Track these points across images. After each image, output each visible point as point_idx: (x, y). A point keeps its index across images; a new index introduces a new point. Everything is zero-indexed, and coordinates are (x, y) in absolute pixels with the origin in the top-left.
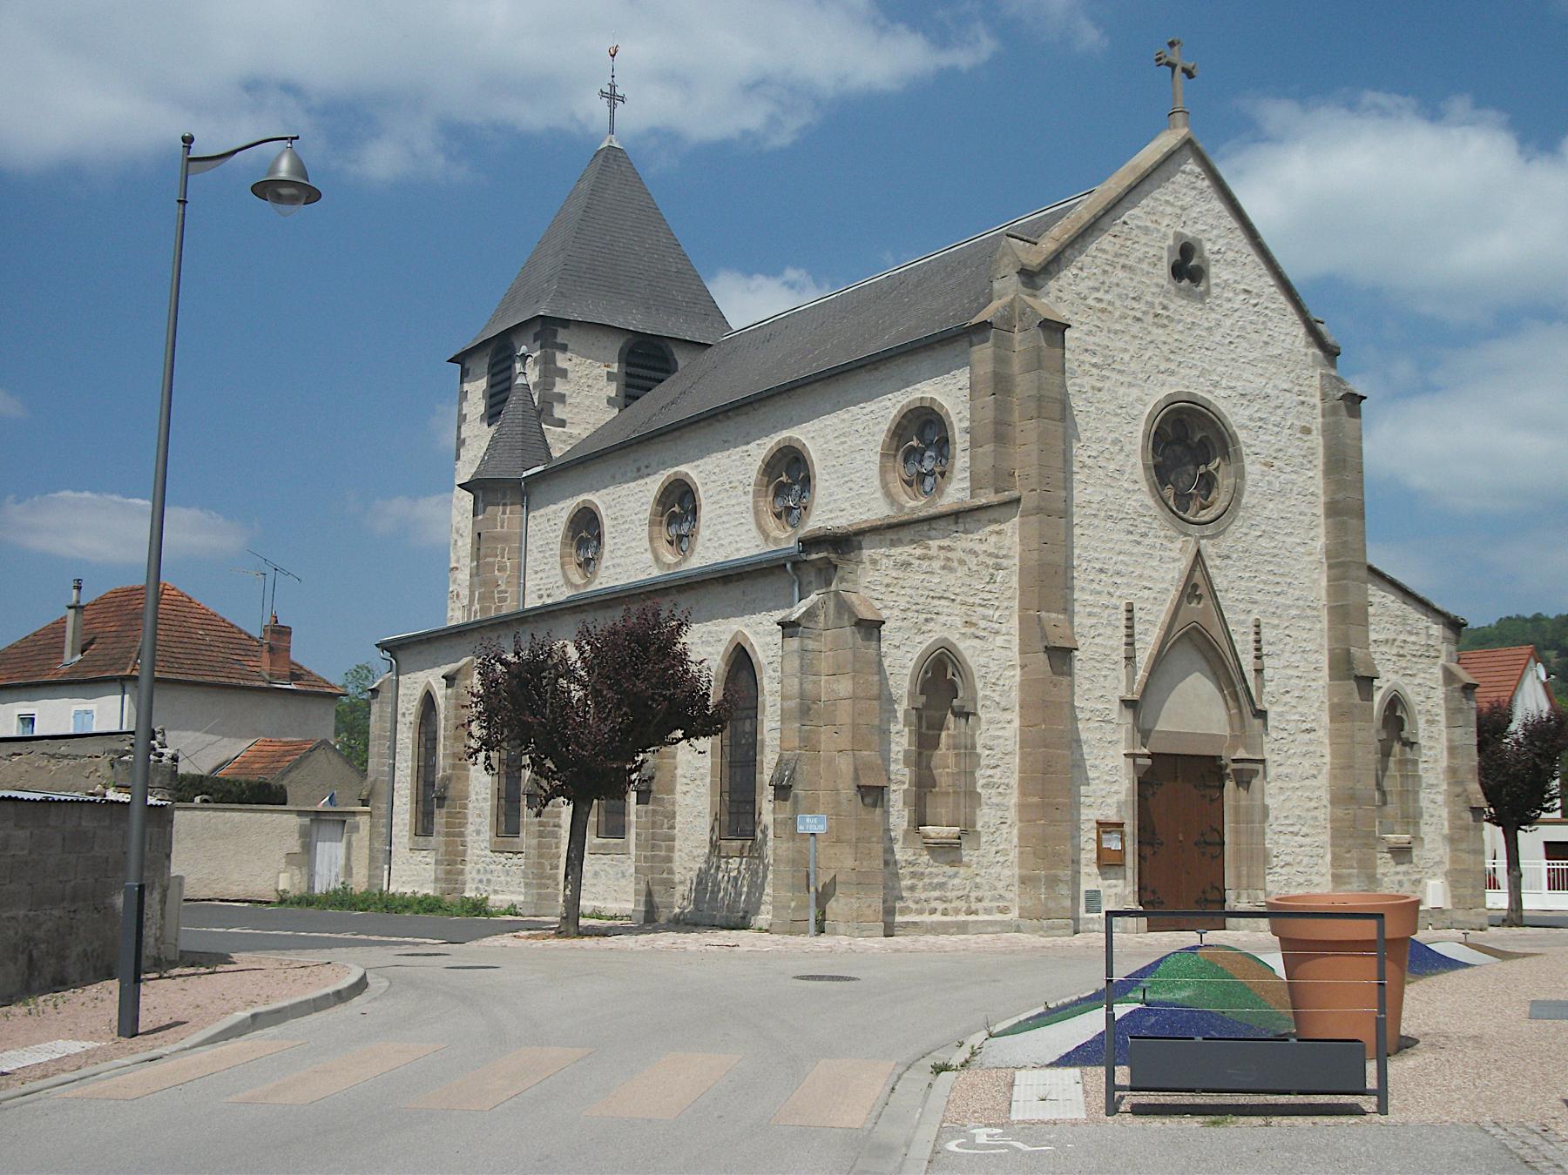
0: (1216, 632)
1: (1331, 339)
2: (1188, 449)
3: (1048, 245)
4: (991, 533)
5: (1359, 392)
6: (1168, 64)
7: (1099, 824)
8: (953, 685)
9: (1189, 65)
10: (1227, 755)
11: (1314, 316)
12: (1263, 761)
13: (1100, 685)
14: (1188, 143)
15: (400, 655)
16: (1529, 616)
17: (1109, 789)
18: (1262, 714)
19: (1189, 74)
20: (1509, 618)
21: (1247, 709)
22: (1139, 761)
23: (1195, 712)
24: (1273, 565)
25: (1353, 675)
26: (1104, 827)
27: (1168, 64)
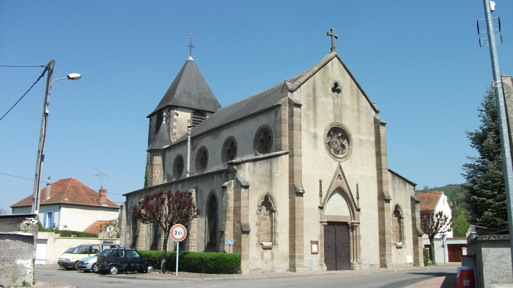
0: (345, 188)
1: (377, 108)
2: (338, 137)
3: (297, 83)
4: (332, 71)
5: (384, 122)
6: (330, 35)
7: (311, 242)
8: (270, 203)
9: (336, 35)
10: (349, 222)
11: (372, 101)
12: (359, 223)
13: (310, 202)
14: (336, 56)
15: (15, 209)
16: (453, 184)
17: (312, 231)
18: (359, 210)
19: (336, 38)
20: (451, 185)
21: (355, 209)
22: (324, 223)
23: (338, 209)
24: (360, 169)
25: (383, 198)
26: (313, 242)
27: (330, 35)
